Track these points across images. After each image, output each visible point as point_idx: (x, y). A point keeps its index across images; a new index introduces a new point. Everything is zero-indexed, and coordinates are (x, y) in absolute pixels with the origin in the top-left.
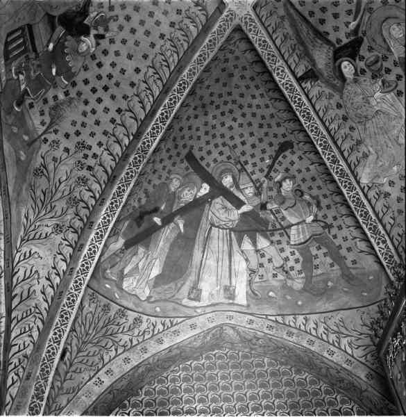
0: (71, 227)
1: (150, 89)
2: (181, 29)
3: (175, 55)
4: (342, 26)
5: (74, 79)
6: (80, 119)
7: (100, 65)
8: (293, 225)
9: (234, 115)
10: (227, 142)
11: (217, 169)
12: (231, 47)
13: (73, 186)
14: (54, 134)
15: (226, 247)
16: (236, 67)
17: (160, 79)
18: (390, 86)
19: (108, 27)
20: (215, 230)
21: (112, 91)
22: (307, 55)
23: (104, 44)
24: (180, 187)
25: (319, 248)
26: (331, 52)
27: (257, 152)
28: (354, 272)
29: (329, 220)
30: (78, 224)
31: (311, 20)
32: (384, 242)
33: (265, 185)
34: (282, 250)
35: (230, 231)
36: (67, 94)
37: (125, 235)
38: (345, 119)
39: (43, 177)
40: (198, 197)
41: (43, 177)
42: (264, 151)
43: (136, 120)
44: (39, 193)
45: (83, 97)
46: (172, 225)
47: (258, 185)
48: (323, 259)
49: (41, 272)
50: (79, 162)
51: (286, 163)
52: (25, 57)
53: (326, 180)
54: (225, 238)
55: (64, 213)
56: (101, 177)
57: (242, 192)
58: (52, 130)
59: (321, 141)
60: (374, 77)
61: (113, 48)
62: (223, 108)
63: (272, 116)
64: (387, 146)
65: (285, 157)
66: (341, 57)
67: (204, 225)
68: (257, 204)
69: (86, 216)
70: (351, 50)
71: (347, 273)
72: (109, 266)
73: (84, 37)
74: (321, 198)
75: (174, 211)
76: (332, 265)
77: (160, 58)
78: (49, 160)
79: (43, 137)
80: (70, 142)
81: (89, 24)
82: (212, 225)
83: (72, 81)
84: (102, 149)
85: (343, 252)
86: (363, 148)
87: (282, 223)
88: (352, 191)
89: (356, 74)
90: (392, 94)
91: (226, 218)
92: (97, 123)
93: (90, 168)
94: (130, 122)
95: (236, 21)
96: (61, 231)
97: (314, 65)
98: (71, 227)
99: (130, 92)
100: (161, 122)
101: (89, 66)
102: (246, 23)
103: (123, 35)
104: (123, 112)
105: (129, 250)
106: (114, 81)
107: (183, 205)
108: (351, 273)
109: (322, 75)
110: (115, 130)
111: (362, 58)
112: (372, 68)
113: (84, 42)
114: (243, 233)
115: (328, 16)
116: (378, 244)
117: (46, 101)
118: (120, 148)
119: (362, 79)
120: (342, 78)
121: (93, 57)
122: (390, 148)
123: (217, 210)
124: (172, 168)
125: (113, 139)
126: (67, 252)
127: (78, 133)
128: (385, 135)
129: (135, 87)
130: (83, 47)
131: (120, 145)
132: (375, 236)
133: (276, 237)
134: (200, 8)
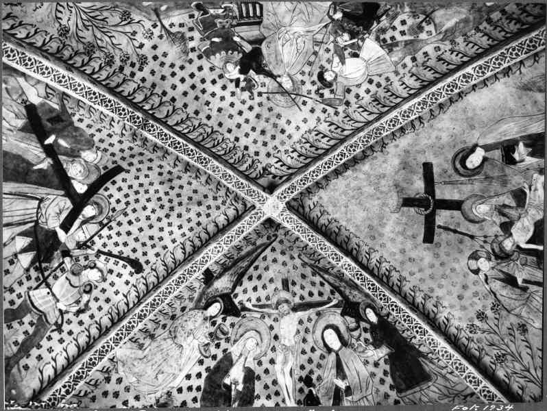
0: (64, 46)
1: (194, 129)
2: (243, 156)
3: (223, 152)
4: (247, 296)
5: (204, 57)
6: (168, 61)
7: (214, 82)
8: (51, 289)
9: (158, 210)
10: (129, 206)
11: (102, 199)
12: (228, 201)
13: (106, 51)
14: (159, 34)
15: (16, 219)
16: (209, 207)
17: (203, 140)
18: (206, 351)
19: (245, 90)
20: (35, 203)
21: (192, 94)
22: (225, 269)
23: (231, 87)
24: (85, 161)
25: (31, 324)
26: (227, 291)
27: (124, 238)
28: (15, 370)
29: (66, 328)
30: (67, 53)
31: (252, 268)
32: (68, 392)
33: (89, 251)
34: (21, 283)
35: (35, 221)
36: (193, 50)
37: (43, 105)
38: (173, 317)
39: (120, 21)
40: (72, 181)
41: (120, 21)
42: (125, 244)
43: (167, 116)
44: (106, 14)
45: (187, 65)
46: (43, 156)
47: (89, 244)
48: (21, 332)
49: (19, 8)
50: (128, 58)
51: (118, 269)
52: (236, 16)
53: (111, 314)
54: (27, 217)
55: (79, 39)
56: (113, 81)
57: (79, 227)
58: (163, 33)
59: (159, 299)
60: (211, 335)
61: (227, 94)
62: (165, 199)
63: (165, 247)
64: (152, 365)
65: (124, 266)
66: (223, 300)
67: (42, 191)
68: (68, 245)
69: (75, 63)
70: (231, 309)
71: (12, 362)
72: (9, 87)
73: (240, 70)
74: (89, 313)
75: (60, 157)
76: (16, 343)
77: (220, 138)
78: (135, 27)
79: (158, 24)
80: (149, 50)
81: (249, 74)
82: (41, 200)
83: (203, 55)
84: (139, 82)
85: (35, 352)
86: (148, 341)
87: (51, 278)
88: (114, 343)
89: (211, 317)
90: (200, 355)
91: (49, 214)
92: (163, 78)
93: (121, 69)
94: (164, 111)
95: (258, 205)
96: (60, 35)
97: (218, 278)
98: (64, 46)
99: (190, 110)
100: (171, 142)
101: (213, 72)
102: (257, 213)
103: (239, 106)
104: (172, 103)
105: (24, 111)
106: (200, 95)
107: (65, 166)
108: (12, 368)
109: (208, 288)
110: (157, 96)
111: (224, 319)
112: (218, 332)
113: (235, 68)
114: (34, 235)
115: (255, 282)
116: (64, 386)
117: (191, 29)
118: (140, 100)
119: (208, 324)
120: (206, 308)
121: (221, 76)
122: (152, 369)
123: (58, 204)
124: (109, 153)
125: (149, 93)
126: (36, 40)
127: (155, 58)
128: (162, 360)
129: (195, 116)
130: (230, 67)
131: (143, 101)
132: (71, 380)
133: (33, 274)
134: (262, 172)
